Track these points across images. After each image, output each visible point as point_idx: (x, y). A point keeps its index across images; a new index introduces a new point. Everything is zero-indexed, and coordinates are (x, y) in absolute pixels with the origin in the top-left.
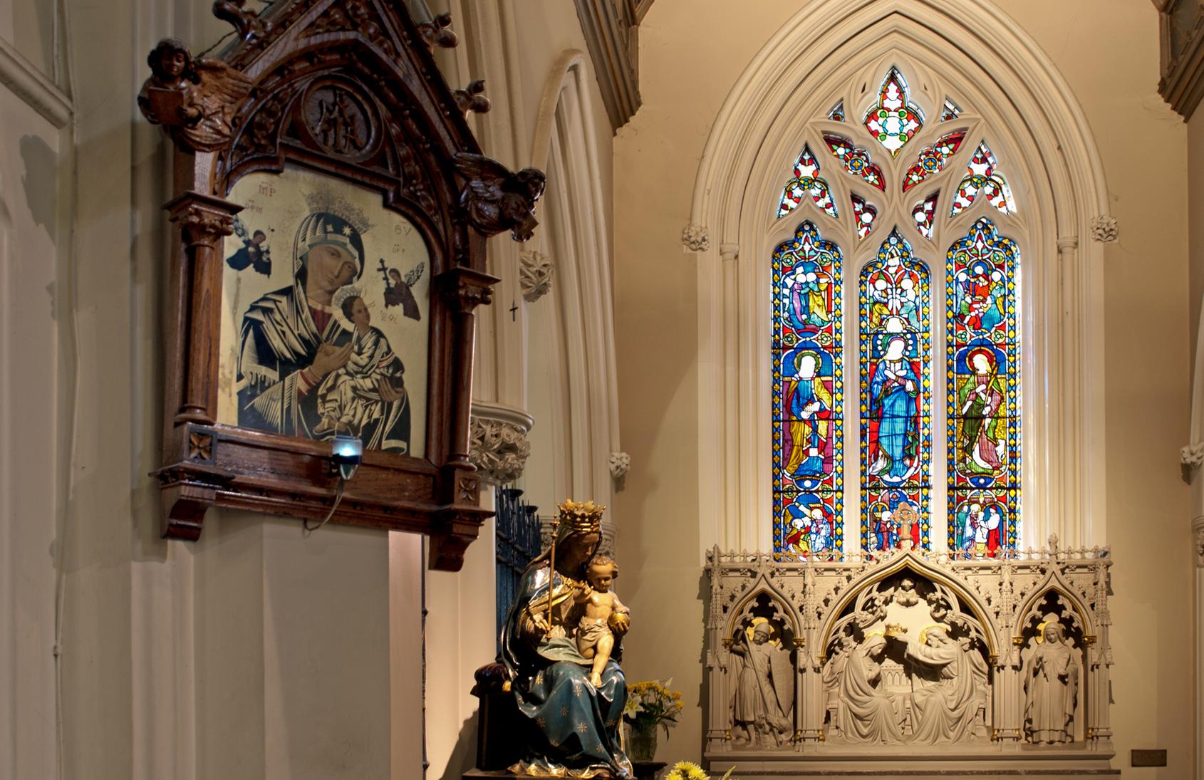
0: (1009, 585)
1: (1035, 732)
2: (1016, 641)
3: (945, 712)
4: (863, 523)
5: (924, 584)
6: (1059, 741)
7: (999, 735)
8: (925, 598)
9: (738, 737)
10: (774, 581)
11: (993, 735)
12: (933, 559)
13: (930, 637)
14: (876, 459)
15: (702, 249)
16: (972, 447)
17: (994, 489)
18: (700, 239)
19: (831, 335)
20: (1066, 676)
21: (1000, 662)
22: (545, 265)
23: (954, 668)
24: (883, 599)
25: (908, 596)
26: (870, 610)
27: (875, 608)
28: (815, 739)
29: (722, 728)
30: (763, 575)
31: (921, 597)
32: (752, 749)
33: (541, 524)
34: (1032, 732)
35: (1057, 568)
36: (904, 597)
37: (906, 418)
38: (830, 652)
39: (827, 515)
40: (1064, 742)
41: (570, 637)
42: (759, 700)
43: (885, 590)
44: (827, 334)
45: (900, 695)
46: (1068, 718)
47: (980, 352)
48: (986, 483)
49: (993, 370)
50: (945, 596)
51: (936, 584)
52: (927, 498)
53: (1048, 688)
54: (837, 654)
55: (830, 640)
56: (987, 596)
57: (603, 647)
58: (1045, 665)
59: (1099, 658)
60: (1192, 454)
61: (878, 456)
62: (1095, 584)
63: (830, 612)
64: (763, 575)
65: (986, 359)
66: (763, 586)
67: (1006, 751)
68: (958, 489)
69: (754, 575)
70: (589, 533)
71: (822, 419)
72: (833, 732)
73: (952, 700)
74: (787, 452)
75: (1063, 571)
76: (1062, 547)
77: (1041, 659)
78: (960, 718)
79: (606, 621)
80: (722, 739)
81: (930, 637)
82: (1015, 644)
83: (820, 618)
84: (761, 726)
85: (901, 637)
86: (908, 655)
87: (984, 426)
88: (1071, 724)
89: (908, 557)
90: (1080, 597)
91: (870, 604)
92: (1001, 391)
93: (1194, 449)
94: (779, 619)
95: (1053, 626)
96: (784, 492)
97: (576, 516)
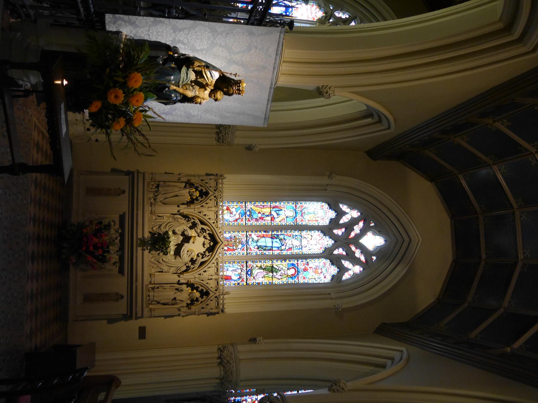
0: (211, 278)
2: (189, 281)
8: (206, 250)
9: (153, 185)
10: (213, 197)
13: (191, 252)
14: (258, 236)
15: (329, 178)
16: (262, 269)
17: (247, 277)
18: (332, 177)
19: (301, 221)
21: (181, 276)
22: (330, 94)
23: (179, 260)
24: (206, 235)
25: (207, 244)
26: (201, 231)
27: (202, 233)
28: (151, 210)
30: (215, 193)
31: (206, 249)
35: (217, 294)
36: (207, 243)
37: (272, 247)
40: (149, 301)
41: (191, 82)
42: (166, 192)
43: (209, 236)
44: (301, 220)
46: (158, 301)
47: (296, 271)
48: (248, 274)
49: (289, 276)
50: (207, 256)
51: (211, 253)
53: (170, 294)
54: (185, 220)
55: (190, 217)
56: (207, 271)
57: (187, 92)
58: (180, 292)
59: (182, 311)
60: (260, 340)
61: (258, 237)
62: (211, 309)
63: (201, 216)
65: (293, 274)
66: (211, 193)
67: (145, 278)
68: (246, 265)
70: (233, 89)
71: (271, 218)
72: (154, 218)
73: (166, 259)
74: (260, 206)
75: (216, 297)
78: (159, 262)
79: (197, 95)
81: (191, 252)
82: (188, 281)
83: (198, 212)
85: (191, 241)
86: (184, 244)
87: (269, 273)
88: (156, 303)
89: (221, 243)
90: (206, 303)
92: (282, 279)
93: (261, 341)
94: (198, 199)
95: (195, 295)
97: (239, 84)
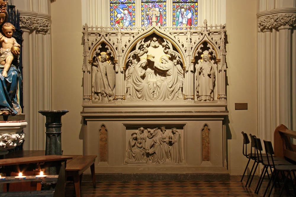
1: (200, 96)
3: (168, 90)
4: (142, 16)
5: (161, 39)
6: (208, 100)
7: (186, 98)
9: (95, 98)
10: (107, 38)
11: (185, 97)
12: (163, 29)
20: (210, 75)
21: (187, 69)
23: (171, 72)
25: (155, 44)
27: (143, 49)
28: (88, 99)
29: (88, 95)
30: (103, 35)
32: (100, 103)
33: (20, 13)
34: (199, 96)
35: (206, 33)
38: (127, 66)
39: (129, 13)
40: (210, 100)
45: (152, 82)
46: (211, 91)
51: (164, 39)
52: (165, 6)
55: (127, 61)
62: (220, 39)
64: (103, 35)
66: (103, 39)
69: (100, 35)
72: (128, 96)
73: (170, 84)
75: (209, 34)
76: (209, 25)
77: (201, 68)
78: (173, 91)
79: (10, 50)
80: (88, 99)
82: (192, 62)
83: (123, 52)
84: (103, 94)
85: (152, 59)
86: (155, 67)
88: (212, 93)
89: (154, 29)
91: (142, 47)
94: (109, 53)
96: (114, 3)
